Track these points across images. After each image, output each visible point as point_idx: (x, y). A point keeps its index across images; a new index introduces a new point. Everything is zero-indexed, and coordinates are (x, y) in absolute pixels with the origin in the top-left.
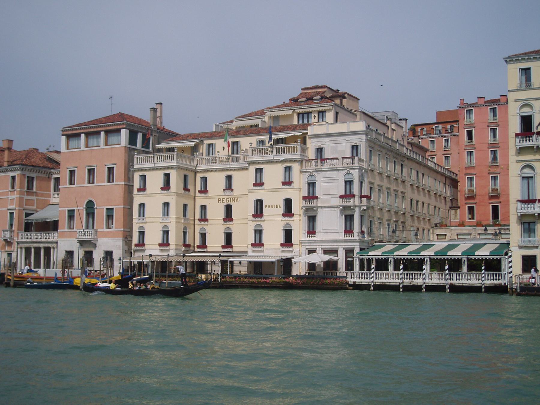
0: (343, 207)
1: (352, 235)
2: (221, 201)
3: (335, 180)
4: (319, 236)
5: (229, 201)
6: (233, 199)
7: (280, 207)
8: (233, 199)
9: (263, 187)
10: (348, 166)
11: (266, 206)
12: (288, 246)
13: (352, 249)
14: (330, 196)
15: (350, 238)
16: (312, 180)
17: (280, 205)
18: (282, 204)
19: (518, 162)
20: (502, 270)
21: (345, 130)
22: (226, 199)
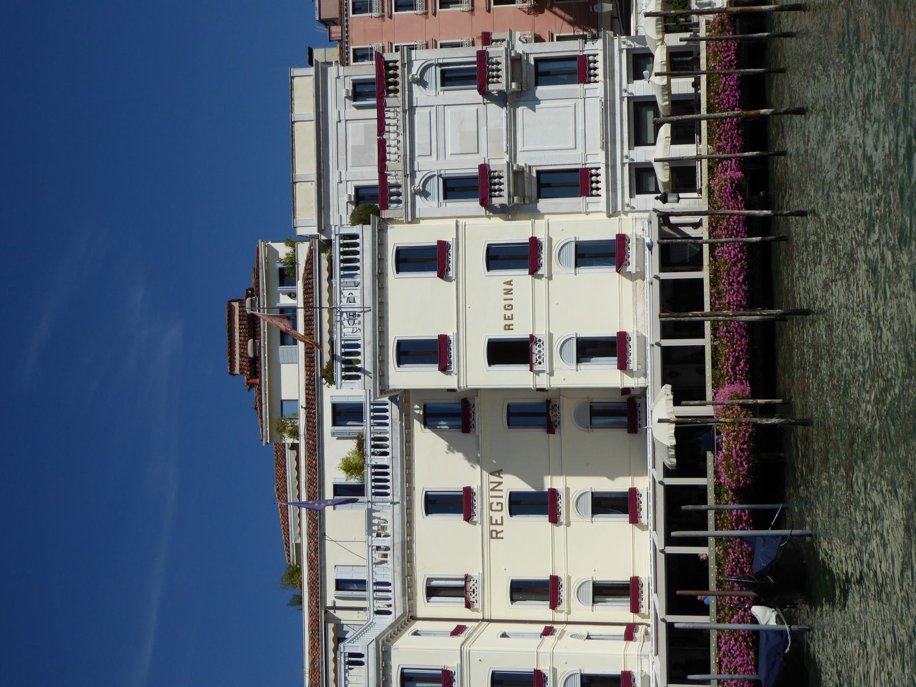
0: (512, 81)
1: (593, 171)
2: (499, 528)
3: (438, 125)
4: (597, 159)
5: (499, 500)
6: (493, 490)
7: (509, 283)
8: (493, 490)
9: (451, 338)
10: (400, 90)
11: (508, 328)
12: (638, 589)
13: (634, 172)
14: (483, 130)
15: (600, 65)
16: (435, 187)
17: (506, 283)
18: (520, 332)
20: (713, 661)
21: (312, 188)
22: (492, 514)
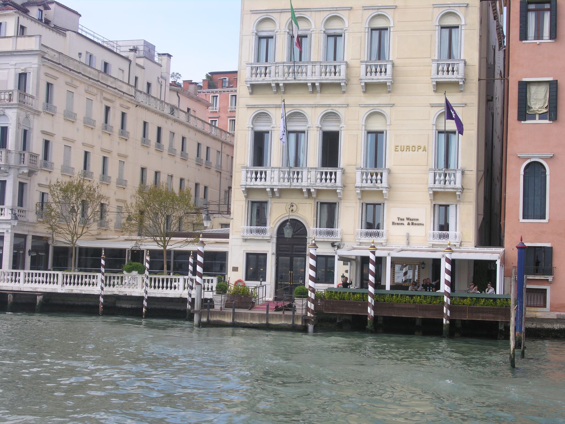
19: (249, 107)
